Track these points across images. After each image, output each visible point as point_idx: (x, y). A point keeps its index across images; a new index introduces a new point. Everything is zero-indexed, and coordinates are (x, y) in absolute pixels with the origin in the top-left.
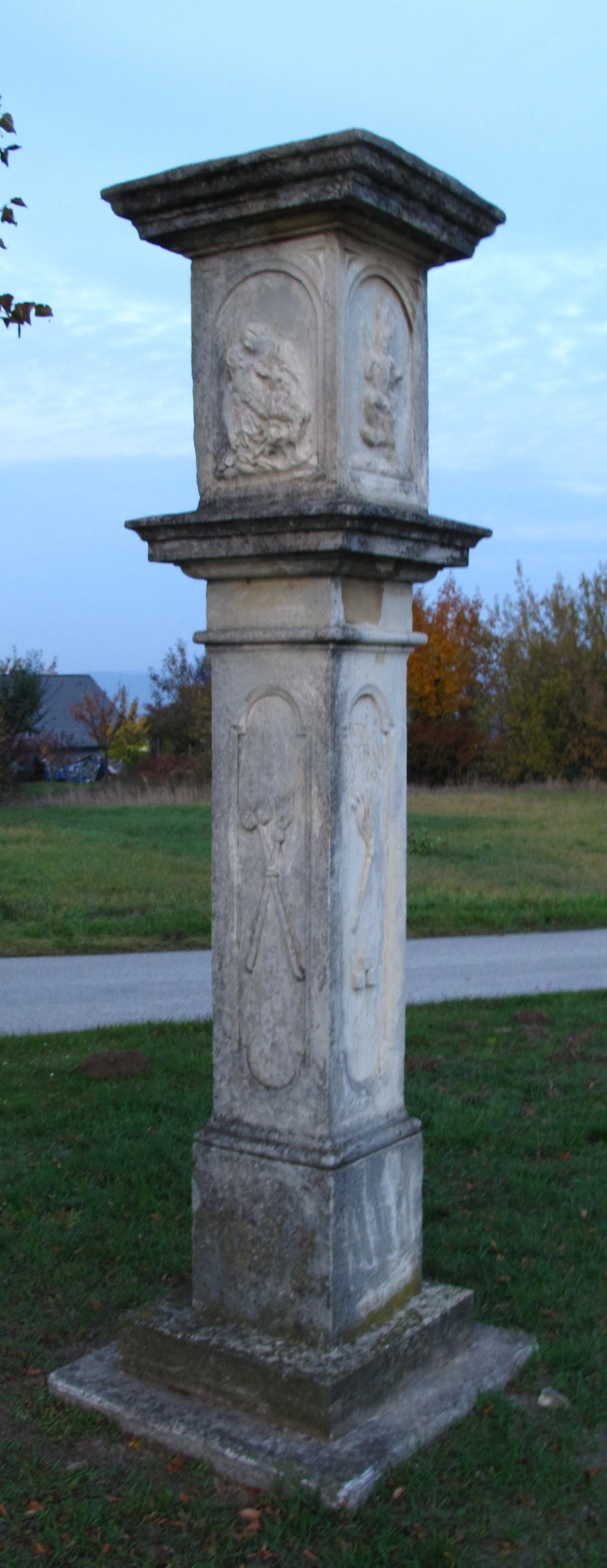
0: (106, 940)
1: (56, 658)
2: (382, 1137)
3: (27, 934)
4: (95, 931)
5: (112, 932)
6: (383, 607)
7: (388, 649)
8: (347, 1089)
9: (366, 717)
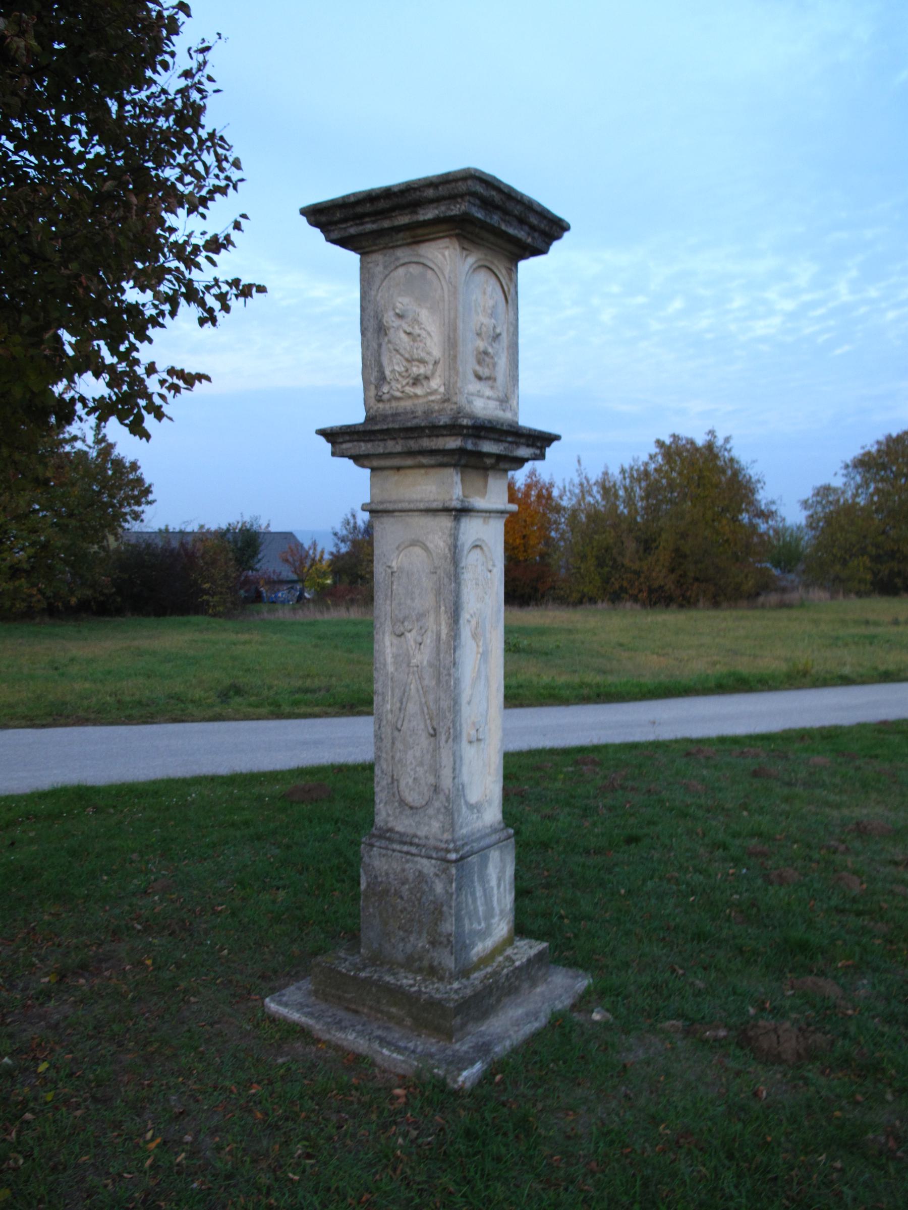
0: (303, 709)
2: (487, 841)
3: (250, 705)
4: (296, 703)
5: (307, 704)
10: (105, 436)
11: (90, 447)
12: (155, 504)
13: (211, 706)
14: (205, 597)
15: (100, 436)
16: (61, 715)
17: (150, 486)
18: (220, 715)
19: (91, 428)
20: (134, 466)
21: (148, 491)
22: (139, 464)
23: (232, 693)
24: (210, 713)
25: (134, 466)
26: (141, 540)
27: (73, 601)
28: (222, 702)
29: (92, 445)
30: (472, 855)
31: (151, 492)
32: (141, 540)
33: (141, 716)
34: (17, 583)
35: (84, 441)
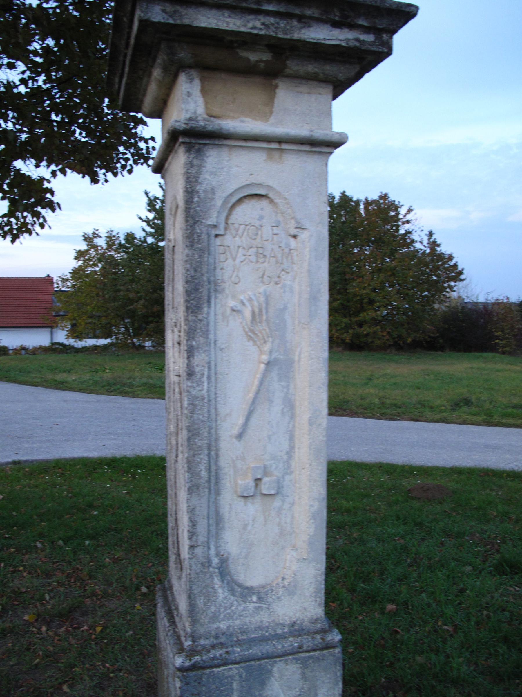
0: (509, 421)
1: (138, 215)
2: (279, 646)
3: (470, 414)
4: (505, 416)
5: (514, 416)
6: (276, 101)
7: (284, 146)
8: (221, 593)
9: (261, 218)
10: (435, 239)
11: (425, 247)
12: (465, 282)
13: (441, 411)
14: (497, 341)
15: (431, 240)
16: (341, 409)
17: (463, 269)
18: (445, 418)
19: (426, 235)
20: (451, 258)
21: (461, 273)
22: (454, 255)
23: (461, 404)
24: (439, 416)
25: (451, 258)
26: (458, 304)
27: (409, 340)
28: (452, 410)
29: (427, 245)
30: (225, 664)
31: (462, 274)
32: (458, 304)
33: (392, 414)
34: (375, 329)
35: (421, 242)
